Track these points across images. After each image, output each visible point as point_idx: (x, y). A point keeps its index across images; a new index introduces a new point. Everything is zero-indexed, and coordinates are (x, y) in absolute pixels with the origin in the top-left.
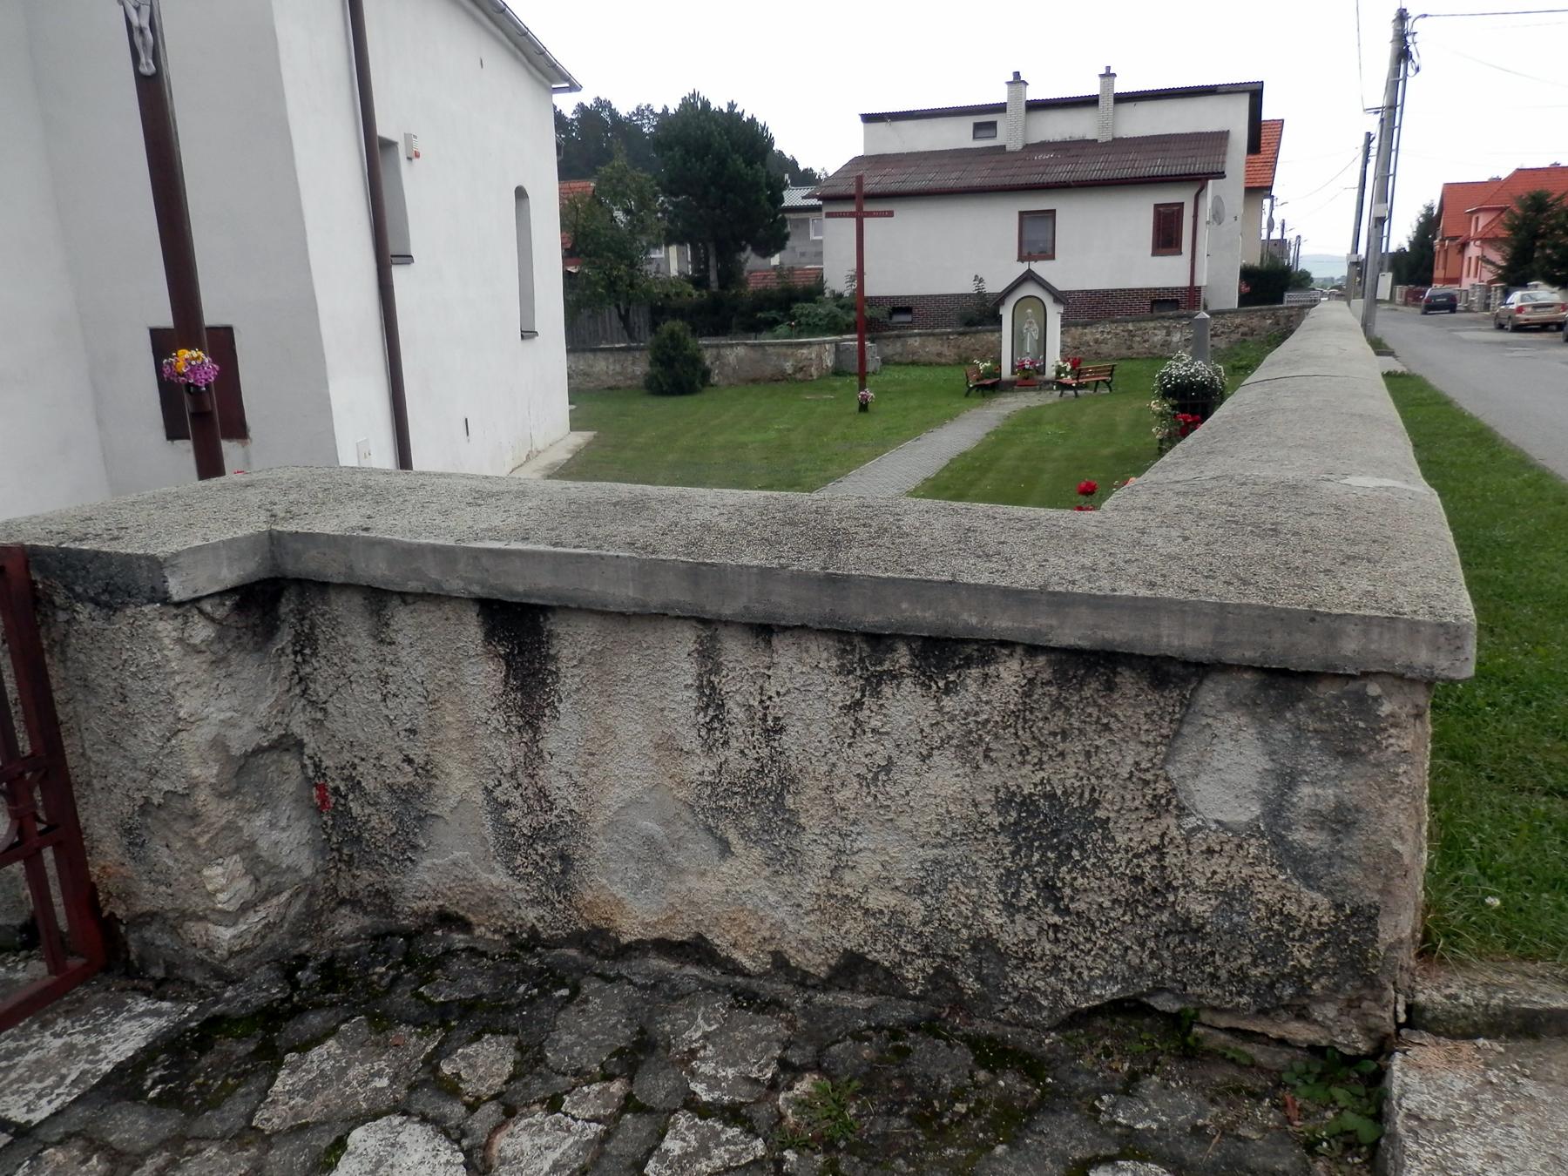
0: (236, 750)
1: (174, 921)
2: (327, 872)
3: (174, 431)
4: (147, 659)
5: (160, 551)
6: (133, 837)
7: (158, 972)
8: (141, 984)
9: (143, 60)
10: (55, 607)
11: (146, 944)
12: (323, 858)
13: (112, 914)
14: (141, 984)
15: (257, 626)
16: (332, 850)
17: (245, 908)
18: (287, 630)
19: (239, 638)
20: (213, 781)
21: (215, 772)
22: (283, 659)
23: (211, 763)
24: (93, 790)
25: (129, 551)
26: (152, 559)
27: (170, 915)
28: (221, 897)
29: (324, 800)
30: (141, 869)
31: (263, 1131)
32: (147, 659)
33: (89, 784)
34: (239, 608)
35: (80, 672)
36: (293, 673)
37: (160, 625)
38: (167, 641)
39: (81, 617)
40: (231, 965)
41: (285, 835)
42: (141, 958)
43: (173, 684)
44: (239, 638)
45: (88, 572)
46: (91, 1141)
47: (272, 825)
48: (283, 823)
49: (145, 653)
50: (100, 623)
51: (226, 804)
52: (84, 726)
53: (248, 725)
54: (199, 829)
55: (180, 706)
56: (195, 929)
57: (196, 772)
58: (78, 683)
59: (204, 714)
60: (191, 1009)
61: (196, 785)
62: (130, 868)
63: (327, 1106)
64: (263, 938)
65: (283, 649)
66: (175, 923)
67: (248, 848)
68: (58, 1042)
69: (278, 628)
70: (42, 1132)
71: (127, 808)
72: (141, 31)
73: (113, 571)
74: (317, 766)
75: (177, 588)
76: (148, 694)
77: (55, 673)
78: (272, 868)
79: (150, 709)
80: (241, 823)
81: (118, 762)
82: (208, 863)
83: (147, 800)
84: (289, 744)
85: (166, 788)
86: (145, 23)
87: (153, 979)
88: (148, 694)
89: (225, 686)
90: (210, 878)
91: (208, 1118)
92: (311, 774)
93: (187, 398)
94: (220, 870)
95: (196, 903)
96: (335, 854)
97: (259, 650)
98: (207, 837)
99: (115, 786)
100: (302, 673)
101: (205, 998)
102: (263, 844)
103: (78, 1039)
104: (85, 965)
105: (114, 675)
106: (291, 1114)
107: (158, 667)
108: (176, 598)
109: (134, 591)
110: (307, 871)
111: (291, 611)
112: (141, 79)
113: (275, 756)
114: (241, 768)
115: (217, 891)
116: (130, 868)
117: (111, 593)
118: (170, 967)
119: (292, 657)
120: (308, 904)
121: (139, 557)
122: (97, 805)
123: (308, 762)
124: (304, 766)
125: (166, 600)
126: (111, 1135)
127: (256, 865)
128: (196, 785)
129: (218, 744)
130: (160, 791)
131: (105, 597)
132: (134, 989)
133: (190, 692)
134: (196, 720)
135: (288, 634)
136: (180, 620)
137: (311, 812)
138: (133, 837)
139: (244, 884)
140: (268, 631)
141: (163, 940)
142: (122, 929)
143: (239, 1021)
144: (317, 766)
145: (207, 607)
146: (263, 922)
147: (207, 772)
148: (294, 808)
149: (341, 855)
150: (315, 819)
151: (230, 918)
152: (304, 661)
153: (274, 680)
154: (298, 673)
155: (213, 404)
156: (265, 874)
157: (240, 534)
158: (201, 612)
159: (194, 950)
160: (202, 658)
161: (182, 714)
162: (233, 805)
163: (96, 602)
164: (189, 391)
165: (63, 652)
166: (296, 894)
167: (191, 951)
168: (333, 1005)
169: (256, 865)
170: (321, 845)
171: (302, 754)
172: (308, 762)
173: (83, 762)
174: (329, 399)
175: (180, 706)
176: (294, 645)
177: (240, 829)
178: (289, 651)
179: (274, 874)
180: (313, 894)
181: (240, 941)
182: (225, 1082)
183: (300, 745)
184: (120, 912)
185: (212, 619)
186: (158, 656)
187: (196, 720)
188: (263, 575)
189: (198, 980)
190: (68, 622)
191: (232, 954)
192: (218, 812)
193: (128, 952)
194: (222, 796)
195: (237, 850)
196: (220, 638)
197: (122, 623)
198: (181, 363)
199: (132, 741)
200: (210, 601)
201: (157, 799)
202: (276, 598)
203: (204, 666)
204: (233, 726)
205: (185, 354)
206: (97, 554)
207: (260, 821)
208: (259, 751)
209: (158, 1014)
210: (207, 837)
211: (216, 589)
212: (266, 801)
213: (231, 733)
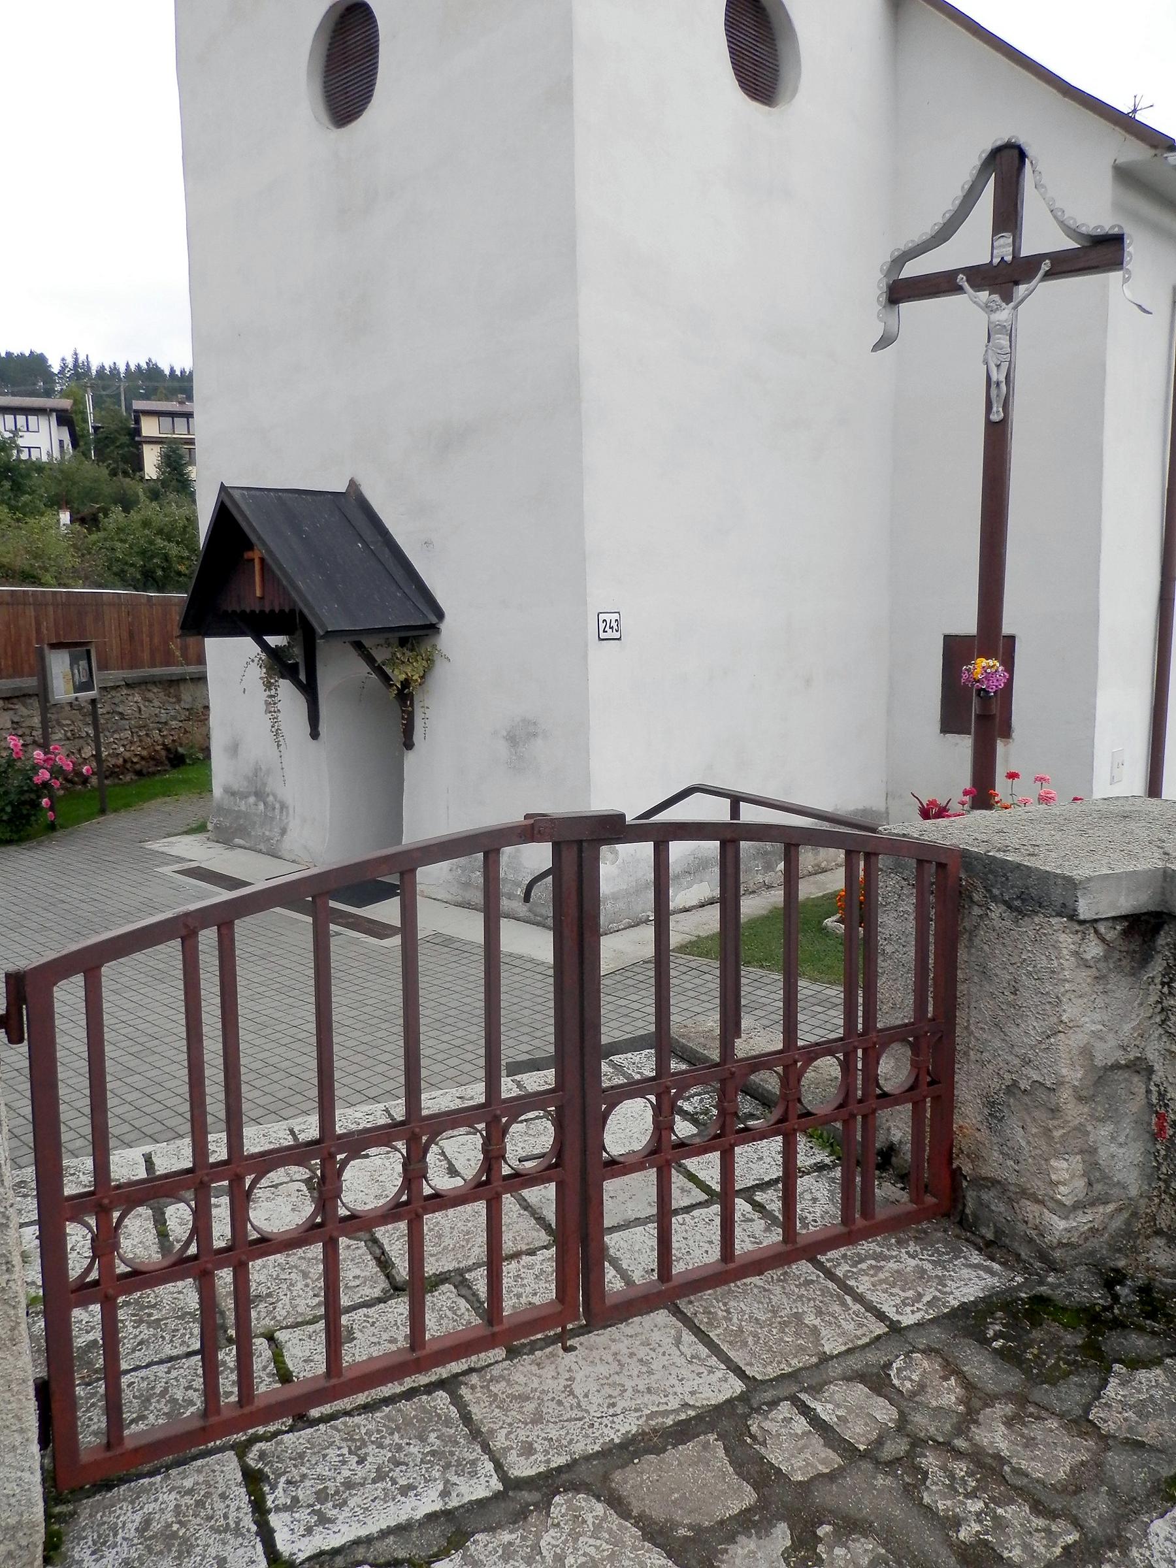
0: (1099, 1063)
1: (1014, 1195)
2: (1150, 1199)
3: (951, 723)
4: (1044, 963)
5: (1078, 874)
6: (994, 1110)
7: (990, 1236)
8: (973, 1238)
9: (995, 409)
10: (972, 901)
11: (982, 1204)
12: (1150, 1185)
13: (960, 1168)
14: (973, 1238)
15: (1135, 952)
16: (1159, 1179)
17: (1079, 1206)
18: (1160, 961)
19: (1120, 960)
20: (1076, 1083)
21: (1079, 1076)
22: (1152, 987)
23: (1078, 1067)
24: (968, 1060)
25: (1048, 869)
26: (1069, 880)
27: (1012, 1188)
28: (1062, 1189)
29: (1162, 1129)
30: (995, 1139)
31: (1099, 1428)
32: (1044, 963)
33: (966, 1054)
34: (1126, 933)
35: (982, 960)
36: (1158, 1002)
37: (1062, 937)
38: (1065, 952)
39: (993, 915)
40: (1057, 1254)
41: (1122, 1151)
42: (975, 1215)
43: (1063, 990)
44: (1120, 960)
45: (1007, 879)
46: (948, 1363)
47: (1113, 1139)
48: (1122, 1139)
49: (1043, 957)
50: (1008, 923)
51: (1081, 1107)
52: (973, 1005)
53: (1112, 1041)
54: (1056, 1123)
55: (1064, 1011)
56: (1031, 1210)
57: (1064, 1071)
58: (977, 968)
59: (1080, 1023)
60: (1019, 1279)
61: (1062, 1083)
62: (983, 1135)
63: (1161, 1435)
64: (1086, 1239)
65: (1153, 978)
66: (1013, 1196)
67: (1089, 1152)
68: (913, 1262)
69: (1152, 957)
70: (911, 1335)
71: (995, 1084)
72: (998, 384)
73: (1030, 882)
74: (1161, 1096)
75: (1085, 910)
76: (1038, 992)
77: (962, 955)
78: (1105, 1178)
79: (1037, 1006)
80: (1089, 1128)
81: (997, 1043)
82: (1057, 1155)
83: (1015, 1083)
84: (1140, 1067)
85: (1035, 1078)
86: (1002, 378)
87: (983, 1237)
88: (1038, 992)
89: (1100, 1002)
90: (1056, 1169)
91: (1046, 1390)
92: (1155, 1101)
93: (975, 699)
94: (1065, 1165)
95: (1037, 1185)
96: (1161, 1183)
97: (1133, 975)
98: (1061, 1132)
99: (989, 1062)
100: (1165, 1004)
101: (1030, 1274)
102: (1103, 1153)
103: (928, 1266)
104: (936, 1205)
105: (1011, 969)
106: (1125, 1425)
107: (1053, 972)
108: (1082, 917)
109: (1045, 904)
110: (1134, 1192)
111: (1168, 944)
112: (989, 423)
113: (1126, 1075)
114: (1100, 1077)
115: (1059, 1183)
116: (983, 1135)
117: (1023, 901)
118: (999, 1232)
119: (1160, 987)
120: (1128, 1223)
121: (1056, 876)
122: (968, 1074)
123: (1153, 1088)
124: (1148, 1091)
125: (1073, 917)
126: (965, 1365)
127: (1094, 1173)
128: (1062, 1083)
129: (1087, 1052)
130: (1029, 1078)
131: (1017, 903)
132: (967, 1240)
133: (1074, 1000)
134: (1076, 1026)
135: (1161, 965)
136: (1080, 935)
137: (1147, 1136)
138: (994, 1110)
139: (1081, 1183)
140: (1145, 959)
141: (999, 1207)
142: (965, 1184)
143: (1064, 1309)
144: (1161, 1096)
145: (1102, 928)
146: (1090, 1225)
147: (1074, 1075)
148: (1133, 1128)
149: (1168, 1187)
150: (1149, 1145)
151: (1066, 1211)
152: (1170, 993)
153: (1141, 1004)
154: (1161, 1003)
155: (995, 709)
156: (1098, 1181)
157: (1140, 868)
158: (1096, 931)
159: (1024, 1227)
160: (1089, 972)
161: (1064, 1018)
162: (1086, 1110)
163: (1009, 906)
164: (978, 695)
165: (970, 940)
166: (1119, 1210)
167: (1021, 1227)
168: (1154, 1333)
169: (1094, 1173)
170: (1149, 1171)
171: (1150, 1079)
172: (1153, 1088)
173: (965, 1034)
174: (1095, 708)
175: (1064, 1011)
176: (1164, 976)
177: (1087, 1133)
178: (1158, 980)
179: (1106, 1184)
180: (1134, 1214)
181: (1068, 1235)
182: (1056, 1364)
183: (1150, 1070)
184: (967, 1169)
185: (1103, 940)
186: (1055, 963)
187: (1076, 1026)
188: (1152, 908)
189: (1023, 1256)
190: (980, 916)
191: (1061, 1245)
192: (1074, 1112)
193: (964, 1205)
194: (1080, 1099)
195: (1081, 1152)
196: (1106, 958)
197: (1028, 927)
198: (979, 670)
199: (1014, 1029)
200: (1105, 923)
201: (1024, 1084)
202: (1156, 930)
203: (1089, 980)
204: (1101, 1039)
205: (982, 662)
206: (1018, 866)
207: (1105, 1131)
208: (1116, 1067)
209: (992, 1273)
210: (1061, 1132)
211: (1113, 914)
212: (1112, 1115)
213: (1099, 1045)
